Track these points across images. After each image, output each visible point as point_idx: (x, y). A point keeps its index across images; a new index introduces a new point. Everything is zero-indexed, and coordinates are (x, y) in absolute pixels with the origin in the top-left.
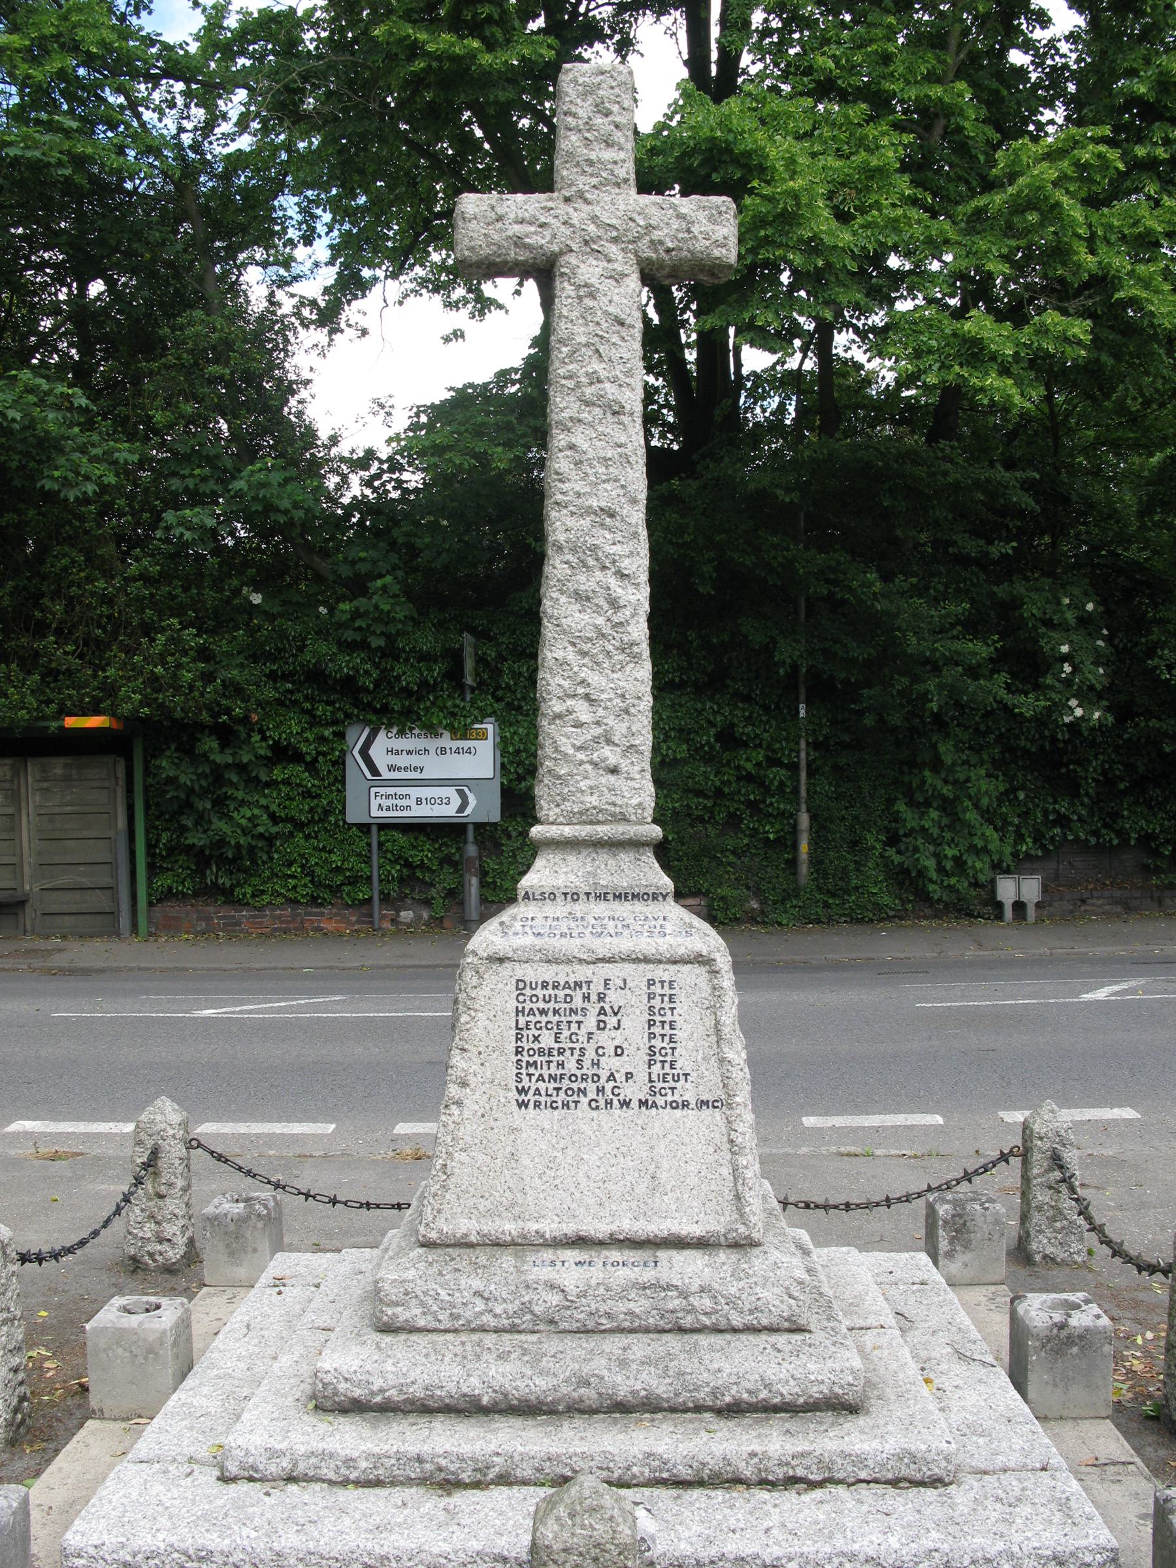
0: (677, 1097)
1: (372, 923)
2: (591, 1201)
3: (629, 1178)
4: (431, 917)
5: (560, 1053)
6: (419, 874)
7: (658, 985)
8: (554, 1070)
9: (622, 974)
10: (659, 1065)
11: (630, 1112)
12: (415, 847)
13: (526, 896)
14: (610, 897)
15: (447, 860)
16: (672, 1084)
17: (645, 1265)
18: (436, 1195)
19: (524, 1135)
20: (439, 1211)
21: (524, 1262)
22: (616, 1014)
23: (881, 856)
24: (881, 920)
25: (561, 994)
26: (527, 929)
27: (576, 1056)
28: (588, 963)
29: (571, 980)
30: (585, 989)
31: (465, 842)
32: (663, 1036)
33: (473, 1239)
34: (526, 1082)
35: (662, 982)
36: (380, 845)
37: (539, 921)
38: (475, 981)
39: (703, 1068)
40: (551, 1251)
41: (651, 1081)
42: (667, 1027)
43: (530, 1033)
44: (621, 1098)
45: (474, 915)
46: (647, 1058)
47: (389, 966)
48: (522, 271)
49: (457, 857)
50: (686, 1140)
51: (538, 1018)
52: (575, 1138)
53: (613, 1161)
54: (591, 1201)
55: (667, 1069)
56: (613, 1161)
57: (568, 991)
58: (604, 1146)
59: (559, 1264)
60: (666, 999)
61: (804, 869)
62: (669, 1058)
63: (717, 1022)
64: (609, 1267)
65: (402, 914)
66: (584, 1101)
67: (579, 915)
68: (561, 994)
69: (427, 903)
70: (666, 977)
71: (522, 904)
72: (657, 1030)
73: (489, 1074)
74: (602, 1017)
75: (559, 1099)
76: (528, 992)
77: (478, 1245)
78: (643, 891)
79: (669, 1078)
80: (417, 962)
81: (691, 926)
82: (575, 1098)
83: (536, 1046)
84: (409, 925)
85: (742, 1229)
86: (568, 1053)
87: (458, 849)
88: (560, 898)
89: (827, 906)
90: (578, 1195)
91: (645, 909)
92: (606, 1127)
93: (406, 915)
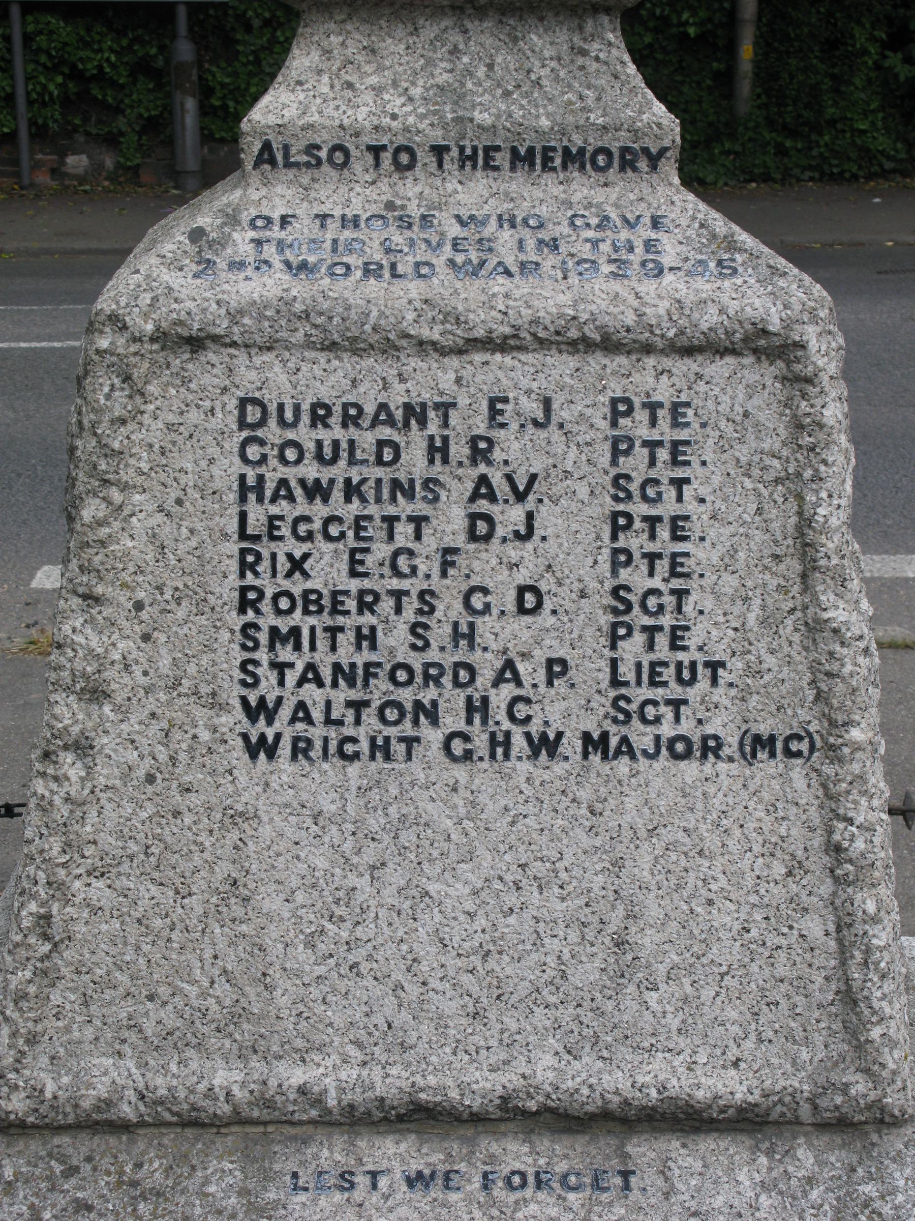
0: (686, 727)
1: (18, 175)
2: (450, 1006)
3: (552, 945)
4: (118, 166)
5: (363, 607)
6: (96, 92)
7: (641, 416)
8: (346, 653)
9: (541, 384)
10: (639, 638)
11: (559, 768)
12: (87, 45)
13: (266, 156)
14: (502, 159)
15: (143, 68)
16: (675, 691)
17: (597, 1185)
18: (21, 997)
19: (266, 831)
20: (32, 1040)
21: (267, 1177)
22: (521, 497)
23: (878, 67)
24: (870, 177)
25: (367, 439)
26: (269, 251)
27: (409, 614)
28: (443, 351)
29: (397, 399)
30: (433, 428)
31: (174, 37)
32: (652, 558)
33: (127, 1111)
34: (268, 686)
35: (653, 407)
36: (27, 39)
37: (303, 228)
38: (120, 404)
39: (761, 648)
40: (340, 1140)
41: (615, 682)
42: (664, 533)
43: (281, 550)
44: (535, 728)
45: (191, 163)
46: (604, 620)
47: (47, 252)
48: (297, 165)
49: (160, 62)
50: (712, 841)
51: (302, 507)
52: (408, 837)
53: (511, 899)
54: (450, 1006)
55: (662, 650)
56: (511, 899)
57: (386, 432)
58: (486, 859)
59: (362, 1181)
60: (663, 454)
61: (745, 88)
62: (667, 621)
63: (805, 522)
64: (499, 1191)
65: (71, 160)
66: (433, 736)
67: (414, 210)
68: (367, 439)
69: (112, 141)
70: (663, 393)
71: (255, 178)
72: (636, 542)
73: (164, 663)
74: (483, 506)
75: (362, 733)
76: (273, 432)
77: (142, 1124)
78: (594, 142)
79: (668, 674)
80: (94, 244)
81: (732, 246)
82: (407, 728)
83: (297, 586)
84: (82, 180)
85: (860, 1086)
86: (387, 605)
87: (162, 48)
88: (360, 164)
89: (781, 151)
90: (413, 991)
91: (599, 196)
92: (491, 809)
93: (76, 162)
